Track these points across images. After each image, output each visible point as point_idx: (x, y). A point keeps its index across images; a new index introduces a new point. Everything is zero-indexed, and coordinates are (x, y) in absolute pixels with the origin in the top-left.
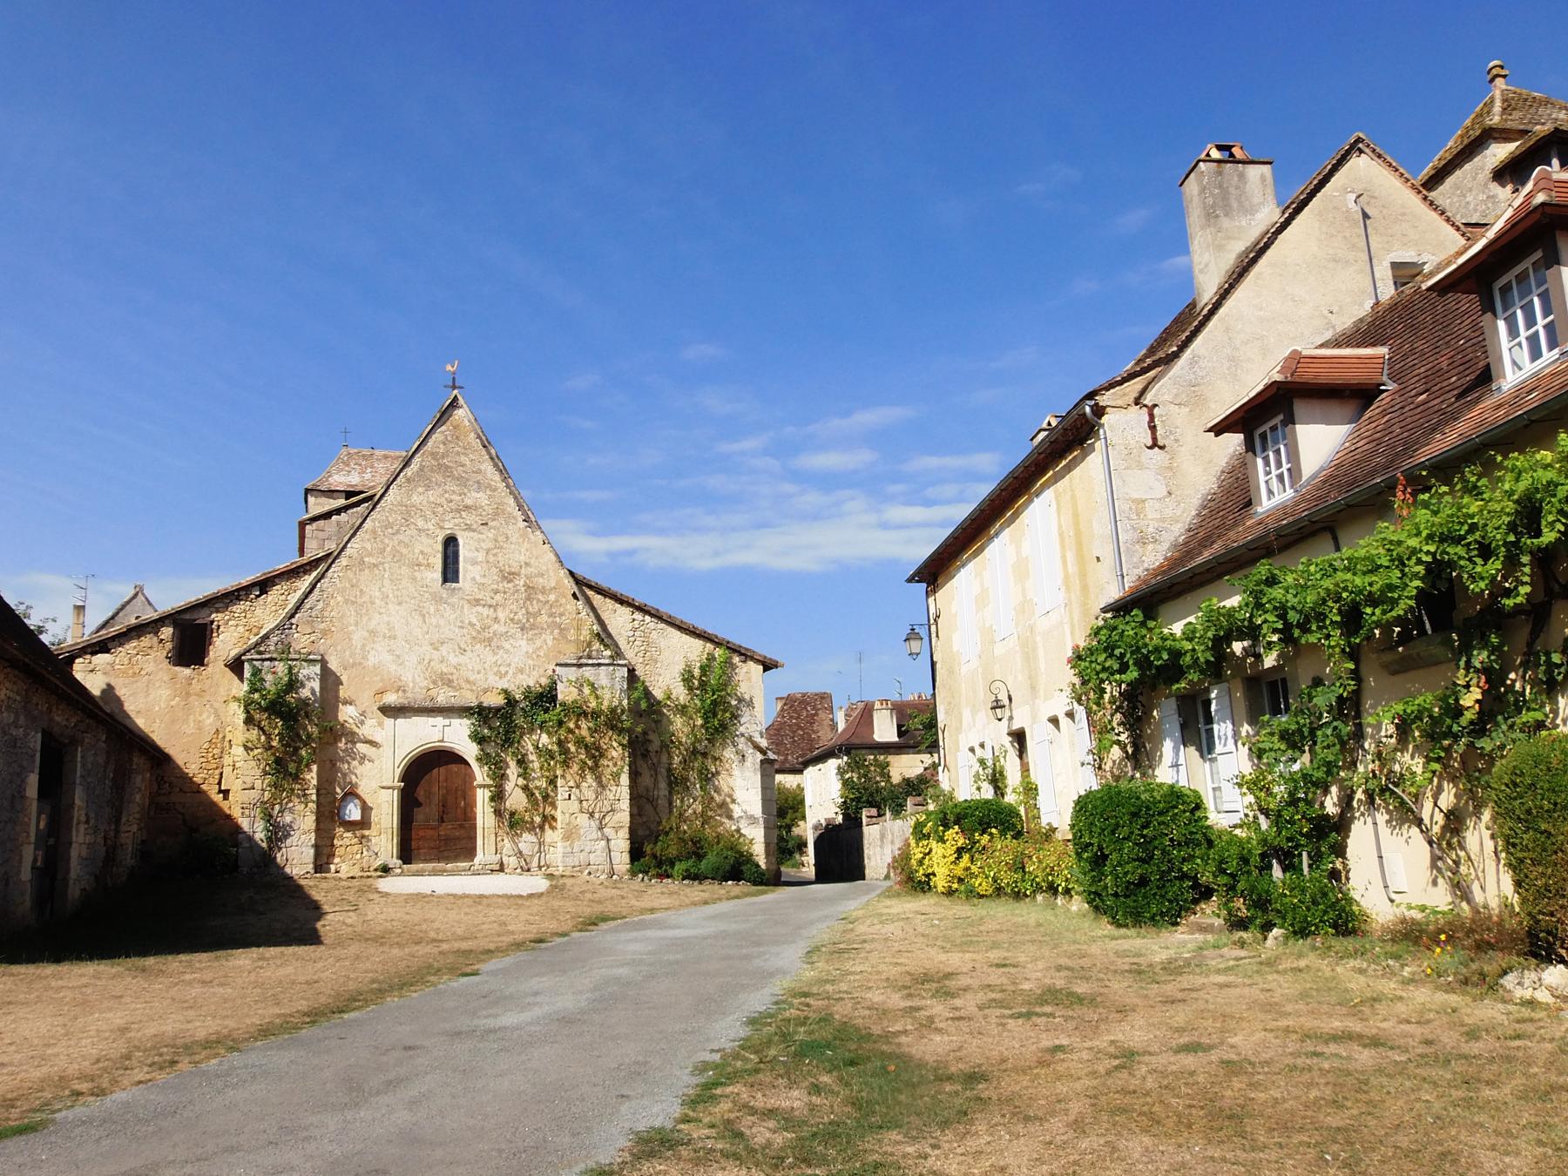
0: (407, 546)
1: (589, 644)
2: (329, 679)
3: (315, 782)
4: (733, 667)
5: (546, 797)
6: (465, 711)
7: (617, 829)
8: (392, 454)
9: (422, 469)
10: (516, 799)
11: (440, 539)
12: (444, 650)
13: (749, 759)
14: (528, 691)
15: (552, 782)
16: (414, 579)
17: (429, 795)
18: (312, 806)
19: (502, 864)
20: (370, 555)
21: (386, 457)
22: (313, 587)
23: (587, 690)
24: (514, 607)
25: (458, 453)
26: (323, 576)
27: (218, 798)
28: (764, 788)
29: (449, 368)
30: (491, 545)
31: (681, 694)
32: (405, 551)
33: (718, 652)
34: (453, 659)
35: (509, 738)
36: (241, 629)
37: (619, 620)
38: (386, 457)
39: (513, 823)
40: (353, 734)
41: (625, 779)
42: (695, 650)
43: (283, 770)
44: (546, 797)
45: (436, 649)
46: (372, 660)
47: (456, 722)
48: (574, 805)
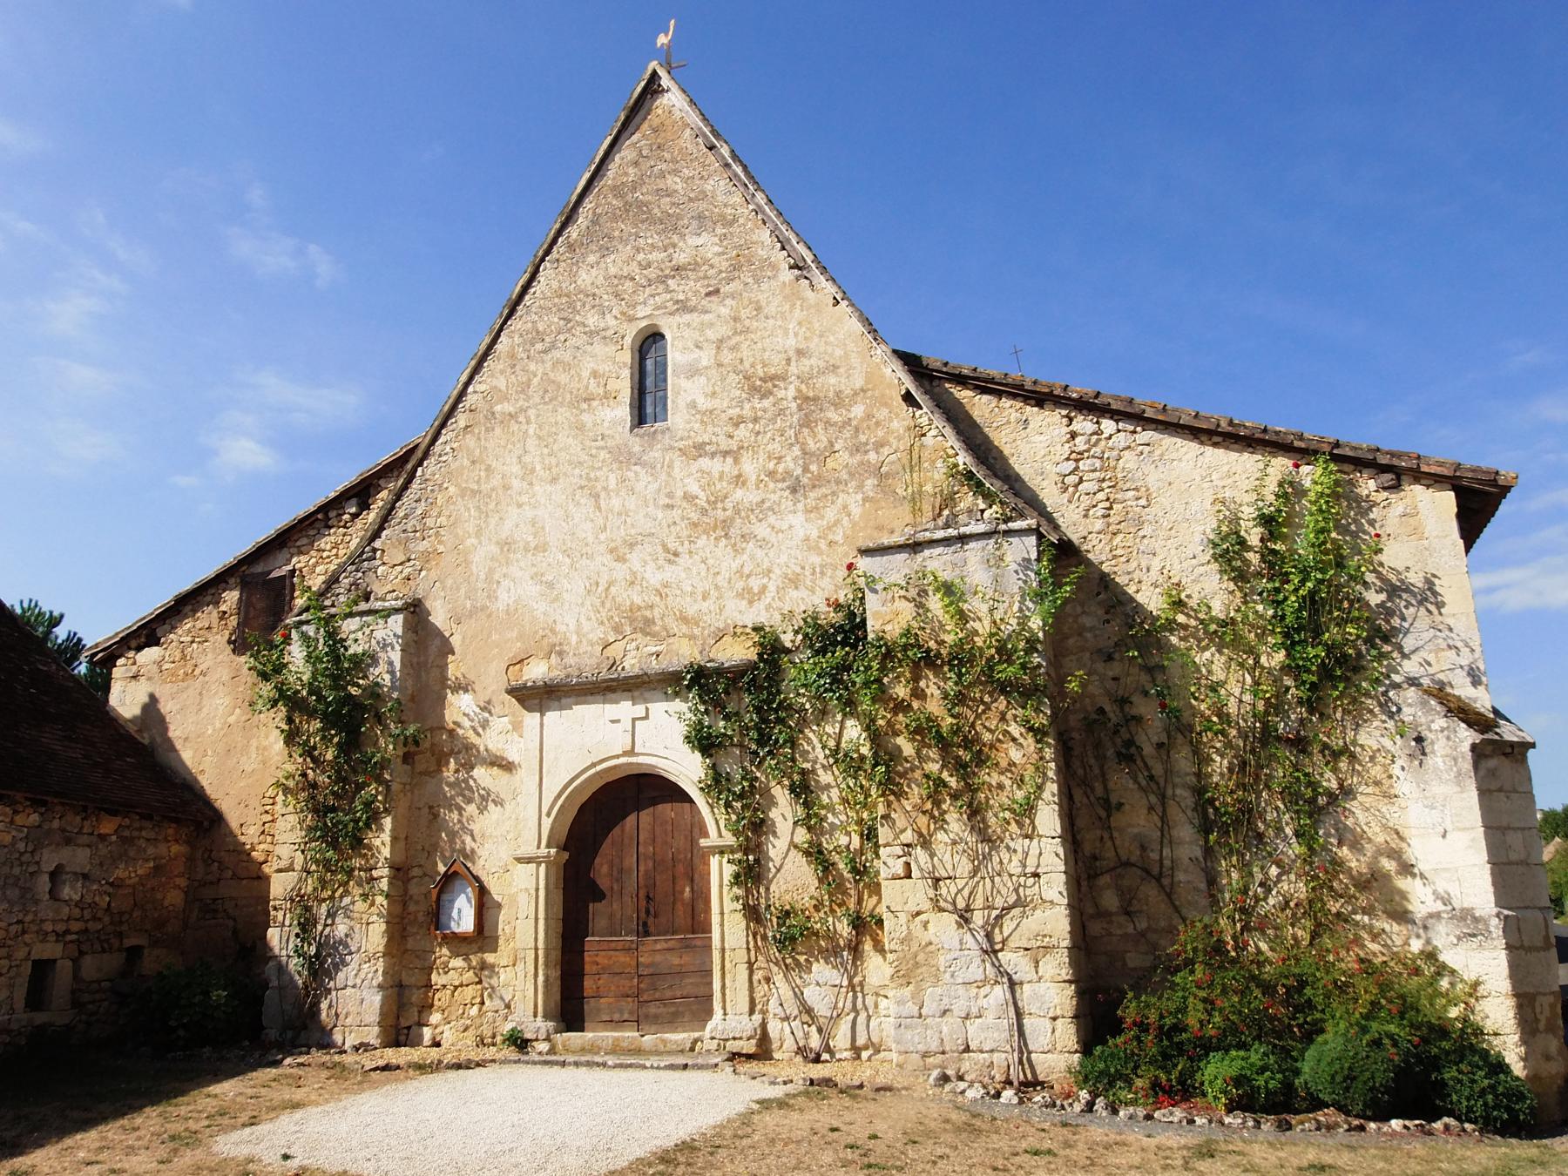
0: (567, 367)
1: (949, 500)
2: (424, 639)
4: (1363, 506)
6: (669, 683)
7: (1036, 953)
10: (792, 879)
12: (635, 558)
13: (1439, 749)
14: (812, 620)
16: (581, 428)
17: (620, 873)
19: (764, 1039)
20: (505, 398)
23: (935, 603)
24: (776, 447)
28: (1496, 831)
30: (724, 330)
31: (1213, 592)
32: (563, 378)
33: (1311, 475)
34: (654, 577)
37: (1035, 442)
39: (789, 938)
40: (468, 747)
41: (1048, 819)
42: (1246, 479)
43: (336, 831)
44: (859, 871)
45: (621, 559)
46: (504, 599)
47: (659, 708)
48: (916, 893)
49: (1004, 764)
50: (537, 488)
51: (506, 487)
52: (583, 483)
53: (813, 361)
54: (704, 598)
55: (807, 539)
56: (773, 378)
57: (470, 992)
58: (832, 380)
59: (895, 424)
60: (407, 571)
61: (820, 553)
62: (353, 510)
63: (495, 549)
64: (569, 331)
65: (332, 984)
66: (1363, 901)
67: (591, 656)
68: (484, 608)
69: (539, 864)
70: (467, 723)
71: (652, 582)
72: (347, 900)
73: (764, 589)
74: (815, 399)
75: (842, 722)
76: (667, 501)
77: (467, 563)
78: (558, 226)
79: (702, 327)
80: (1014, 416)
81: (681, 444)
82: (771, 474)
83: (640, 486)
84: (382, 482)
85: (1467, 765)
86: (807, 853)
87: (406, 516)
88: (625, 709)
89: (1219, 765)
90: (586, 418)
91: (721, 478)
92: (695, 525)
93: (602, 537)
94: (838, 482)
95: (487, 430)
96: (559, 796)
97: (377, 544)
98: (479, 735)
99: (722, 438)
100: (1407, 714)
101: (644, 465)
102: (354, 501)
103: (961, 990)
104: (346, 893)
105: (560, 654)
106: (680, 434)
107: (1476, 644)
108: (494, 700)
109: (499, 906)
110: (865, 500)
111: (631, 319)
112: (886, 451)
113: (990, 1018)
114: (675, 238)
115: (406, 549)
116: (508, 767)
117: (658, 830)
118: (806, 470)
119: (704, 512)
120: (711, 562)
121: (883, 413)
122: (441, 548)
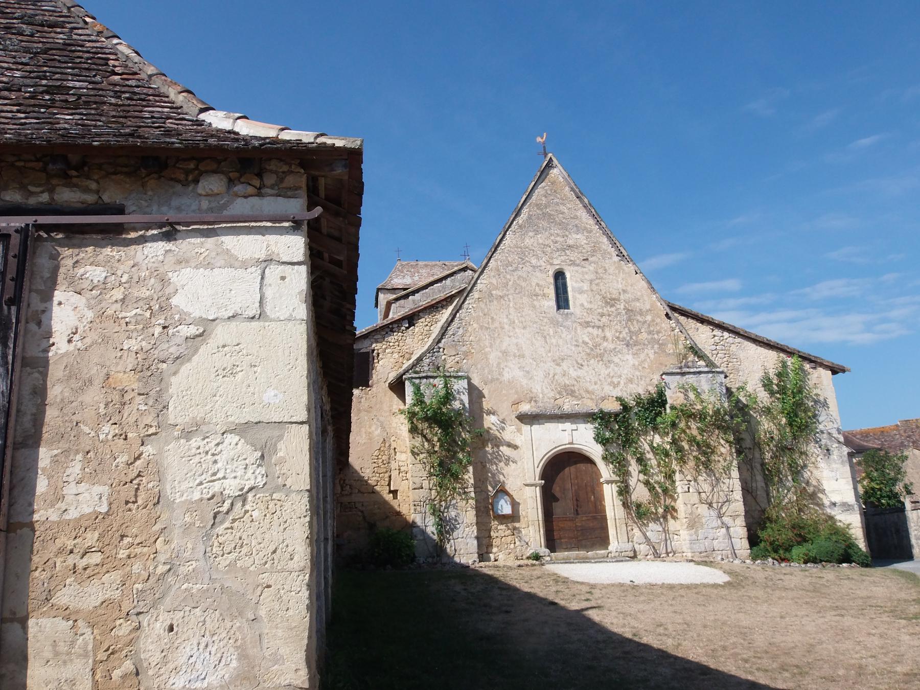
0: (525, 280)
1: (685, 357)
2: (475, 393)
6: (589, 417)
7: (734, 517)
10: (640, 493)
12: (565, 365)
13: (835, 455)
16: (534, 307)
20: (497, 288)
23: (692, 396)
24: (618, 327)
30: (592, 276)
31: (763, 397)
32: (523, 284)
33: (790, 361)
34: (573, 373)
41: (735, 474)
42: (771, 359)
43: (445, 471)
45: (558, 365)
51: (502, 328)
55: (634, 365)
56: (614, 299)
60: (457, 359)
63: (500, 354)
68: (497, 379)
70: (494, 428)
72: (454, 502)
73: (619, 383)
74: (632, 311)
77: (487, 359)
79: (583, 273)
82: (618, 338)
83: (564, 336)
85: (846, 458)
87: (454, 335)
88: (568, 426)
89: (768, 455)
90: (535, 303)
92: (589, 354)
97: (440, 345)
99: (596, 321)
100: (823, 442)
101: (564, 327)
103: (711, 531)
105: (535, 401)
109: (519, 504)
110: (655, 353)
111: (552, 264)
113: (721, 539)
115: (456, 349)
116: (515, 447)
118: (631, 338)
119: (592, 350)
121: (658, 320)
122: (473, 351)
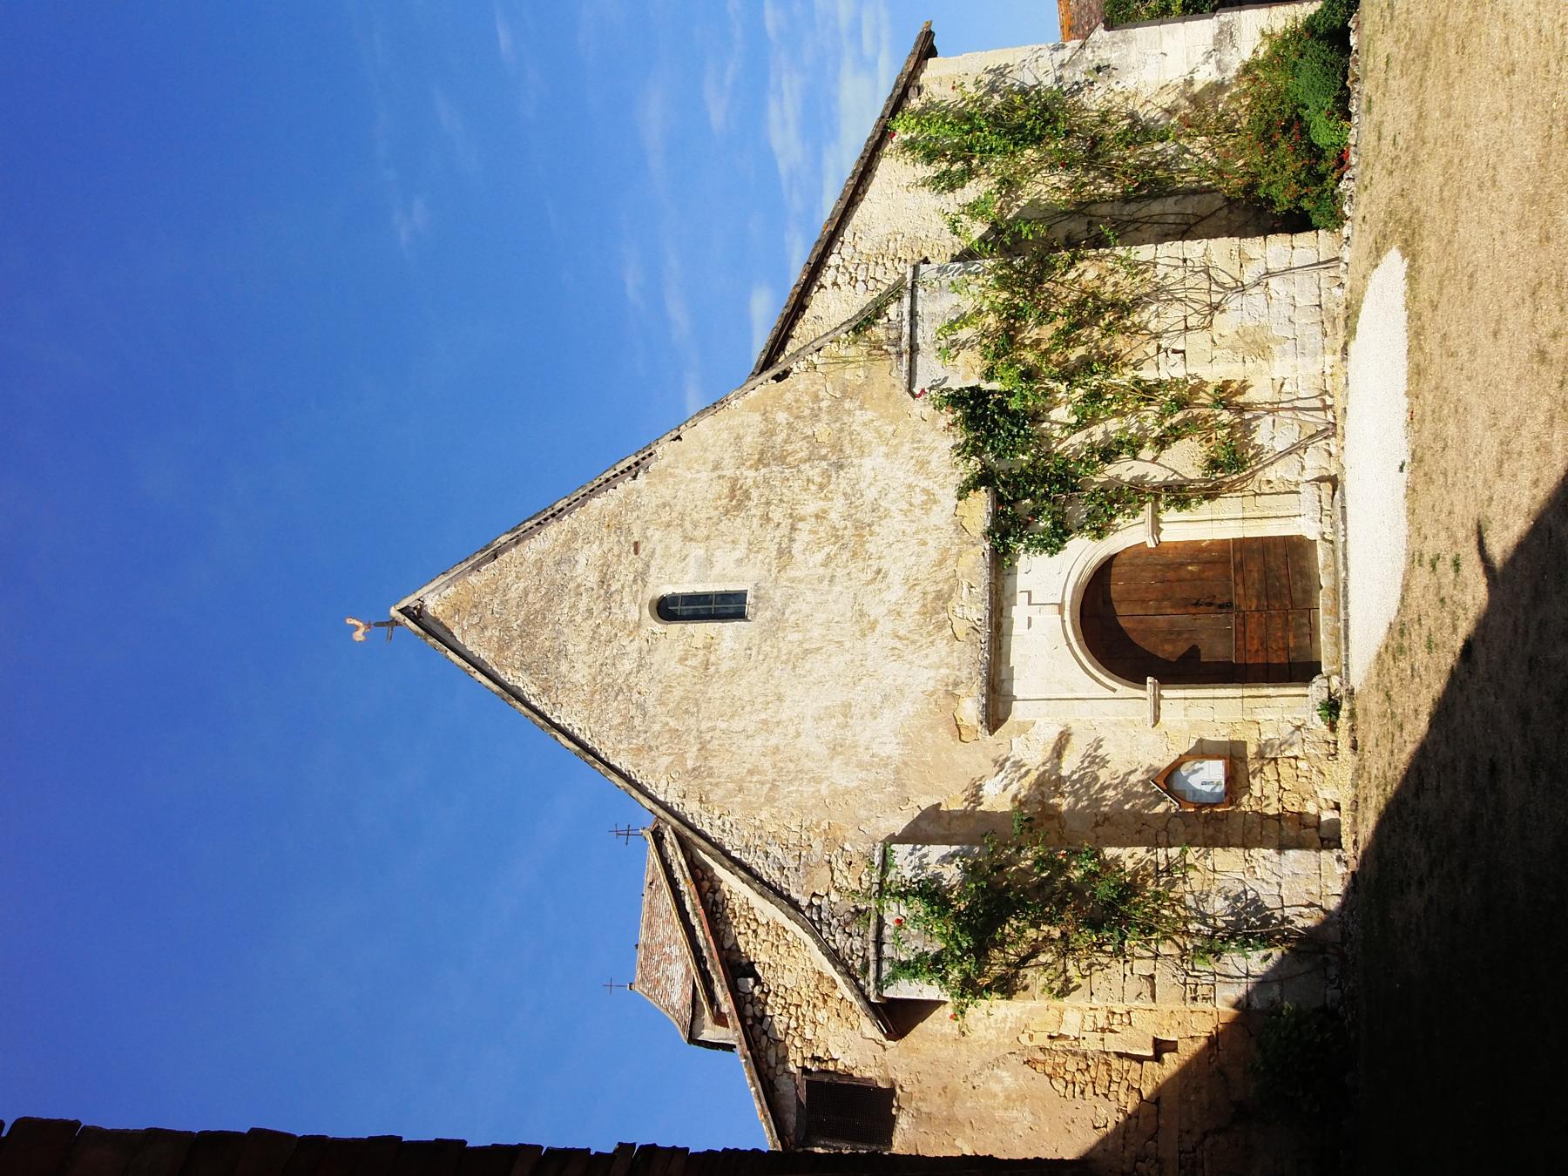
0: (668, 689)
3: (1141, 851)
5: (1181, 403)
6: (1000, 562)
8: (646, 916)
9: (525, 667)
10: (1185, 460)
11: (659, 627)
12: (875, 611)
13: (1106, 55)
15: (1147, 392)
16: (733, 672)
17: (1173, 633)
18: (1192, 855)
20: (681, 756)
21: (650, 926)
22: (738, 865)
23: (965, 333)
24: (797, 485)
25: (504, 603)
26: (718, 847)
27: (1172, 1063)
29: (359, 636)
30: (676, 535)
32: (678, 693)
34: (896, 593)
35: (1061, 479)
36: (821, 1015)
38: (650, 926)
40: (1040, 782)
41: (1145, 252)
42: (894, 171)
43: (1112, 915)
45: (873, 626)
46: (891, 749)
48: (1197, 342)
49: (1097, 283)
50: (784, 717)
51: (777, 749)
52: (790, 666)
53: (727, 456)
54: (925, 544)
56: (733, 490)
57: (1285, 770)
58: (749, 439)
59: (801, 387)
60: (841, 865)
61: (902, 444)
62: (751, 981)
63: (838, 760)
64: (630, 689)
65: (1278, 914)
66: (1209, 108)
67: (963, 652)
68: (897, 771)
69: (1161, 697)
70: (1014, 788)
71: (901, 594)
74: (762, 453)
75: (1052, 423)
76: (826, 582)
77: (847, 792)
78: (518, 704)
80: (809, 326)
81: (774, 571)
82: (821, 487)
83: (806, 609)
84: (727, 944)
85: (1118, 35)
86: (1162, 448)
88: (1019, 613)
89: (1107, 188)
90: (724, 668)
91: (815, 533)
92: (854, 554)
93: (848, 645)
94: (842, 430)
95: (710, 775)
96: (1097, 680)
97: (804, 902)
98: (1027, 772)
99: (778, 533)
100: (1080, 77)
101: (786, 605)
102: (741, 981)
103: (1274, 310)
104: (1180, 900)
105: (956, 684)
106: (765, 573)
107: (1036, 48)
108: (994, 756)
109: (1201, 741)
110: (861, 408)
111: (639, 625)
112: (822, 394)
113: (1294, 290)
114: (572, 585)
117: (1135, 597)
118: (824, 458)
120: (892, 539)
121: (789, 397)
122: (824, 825)
